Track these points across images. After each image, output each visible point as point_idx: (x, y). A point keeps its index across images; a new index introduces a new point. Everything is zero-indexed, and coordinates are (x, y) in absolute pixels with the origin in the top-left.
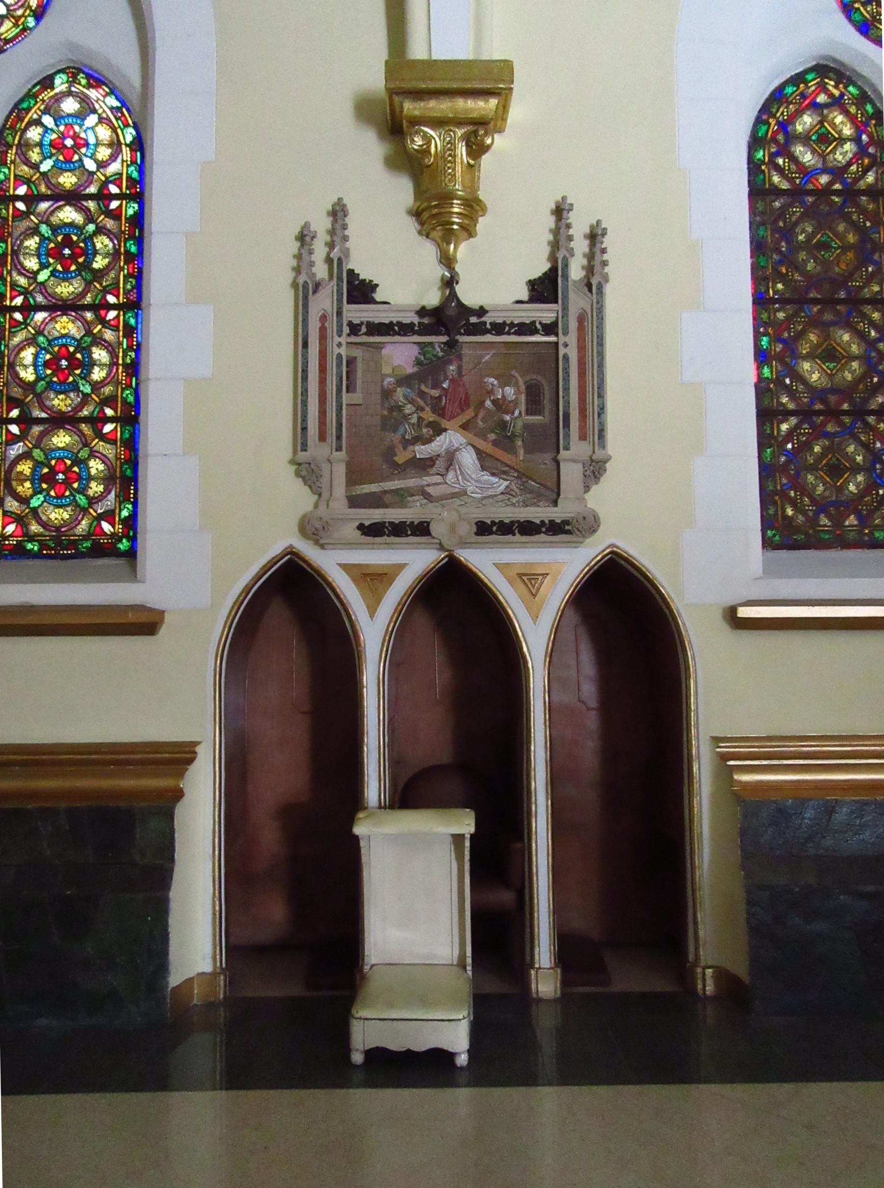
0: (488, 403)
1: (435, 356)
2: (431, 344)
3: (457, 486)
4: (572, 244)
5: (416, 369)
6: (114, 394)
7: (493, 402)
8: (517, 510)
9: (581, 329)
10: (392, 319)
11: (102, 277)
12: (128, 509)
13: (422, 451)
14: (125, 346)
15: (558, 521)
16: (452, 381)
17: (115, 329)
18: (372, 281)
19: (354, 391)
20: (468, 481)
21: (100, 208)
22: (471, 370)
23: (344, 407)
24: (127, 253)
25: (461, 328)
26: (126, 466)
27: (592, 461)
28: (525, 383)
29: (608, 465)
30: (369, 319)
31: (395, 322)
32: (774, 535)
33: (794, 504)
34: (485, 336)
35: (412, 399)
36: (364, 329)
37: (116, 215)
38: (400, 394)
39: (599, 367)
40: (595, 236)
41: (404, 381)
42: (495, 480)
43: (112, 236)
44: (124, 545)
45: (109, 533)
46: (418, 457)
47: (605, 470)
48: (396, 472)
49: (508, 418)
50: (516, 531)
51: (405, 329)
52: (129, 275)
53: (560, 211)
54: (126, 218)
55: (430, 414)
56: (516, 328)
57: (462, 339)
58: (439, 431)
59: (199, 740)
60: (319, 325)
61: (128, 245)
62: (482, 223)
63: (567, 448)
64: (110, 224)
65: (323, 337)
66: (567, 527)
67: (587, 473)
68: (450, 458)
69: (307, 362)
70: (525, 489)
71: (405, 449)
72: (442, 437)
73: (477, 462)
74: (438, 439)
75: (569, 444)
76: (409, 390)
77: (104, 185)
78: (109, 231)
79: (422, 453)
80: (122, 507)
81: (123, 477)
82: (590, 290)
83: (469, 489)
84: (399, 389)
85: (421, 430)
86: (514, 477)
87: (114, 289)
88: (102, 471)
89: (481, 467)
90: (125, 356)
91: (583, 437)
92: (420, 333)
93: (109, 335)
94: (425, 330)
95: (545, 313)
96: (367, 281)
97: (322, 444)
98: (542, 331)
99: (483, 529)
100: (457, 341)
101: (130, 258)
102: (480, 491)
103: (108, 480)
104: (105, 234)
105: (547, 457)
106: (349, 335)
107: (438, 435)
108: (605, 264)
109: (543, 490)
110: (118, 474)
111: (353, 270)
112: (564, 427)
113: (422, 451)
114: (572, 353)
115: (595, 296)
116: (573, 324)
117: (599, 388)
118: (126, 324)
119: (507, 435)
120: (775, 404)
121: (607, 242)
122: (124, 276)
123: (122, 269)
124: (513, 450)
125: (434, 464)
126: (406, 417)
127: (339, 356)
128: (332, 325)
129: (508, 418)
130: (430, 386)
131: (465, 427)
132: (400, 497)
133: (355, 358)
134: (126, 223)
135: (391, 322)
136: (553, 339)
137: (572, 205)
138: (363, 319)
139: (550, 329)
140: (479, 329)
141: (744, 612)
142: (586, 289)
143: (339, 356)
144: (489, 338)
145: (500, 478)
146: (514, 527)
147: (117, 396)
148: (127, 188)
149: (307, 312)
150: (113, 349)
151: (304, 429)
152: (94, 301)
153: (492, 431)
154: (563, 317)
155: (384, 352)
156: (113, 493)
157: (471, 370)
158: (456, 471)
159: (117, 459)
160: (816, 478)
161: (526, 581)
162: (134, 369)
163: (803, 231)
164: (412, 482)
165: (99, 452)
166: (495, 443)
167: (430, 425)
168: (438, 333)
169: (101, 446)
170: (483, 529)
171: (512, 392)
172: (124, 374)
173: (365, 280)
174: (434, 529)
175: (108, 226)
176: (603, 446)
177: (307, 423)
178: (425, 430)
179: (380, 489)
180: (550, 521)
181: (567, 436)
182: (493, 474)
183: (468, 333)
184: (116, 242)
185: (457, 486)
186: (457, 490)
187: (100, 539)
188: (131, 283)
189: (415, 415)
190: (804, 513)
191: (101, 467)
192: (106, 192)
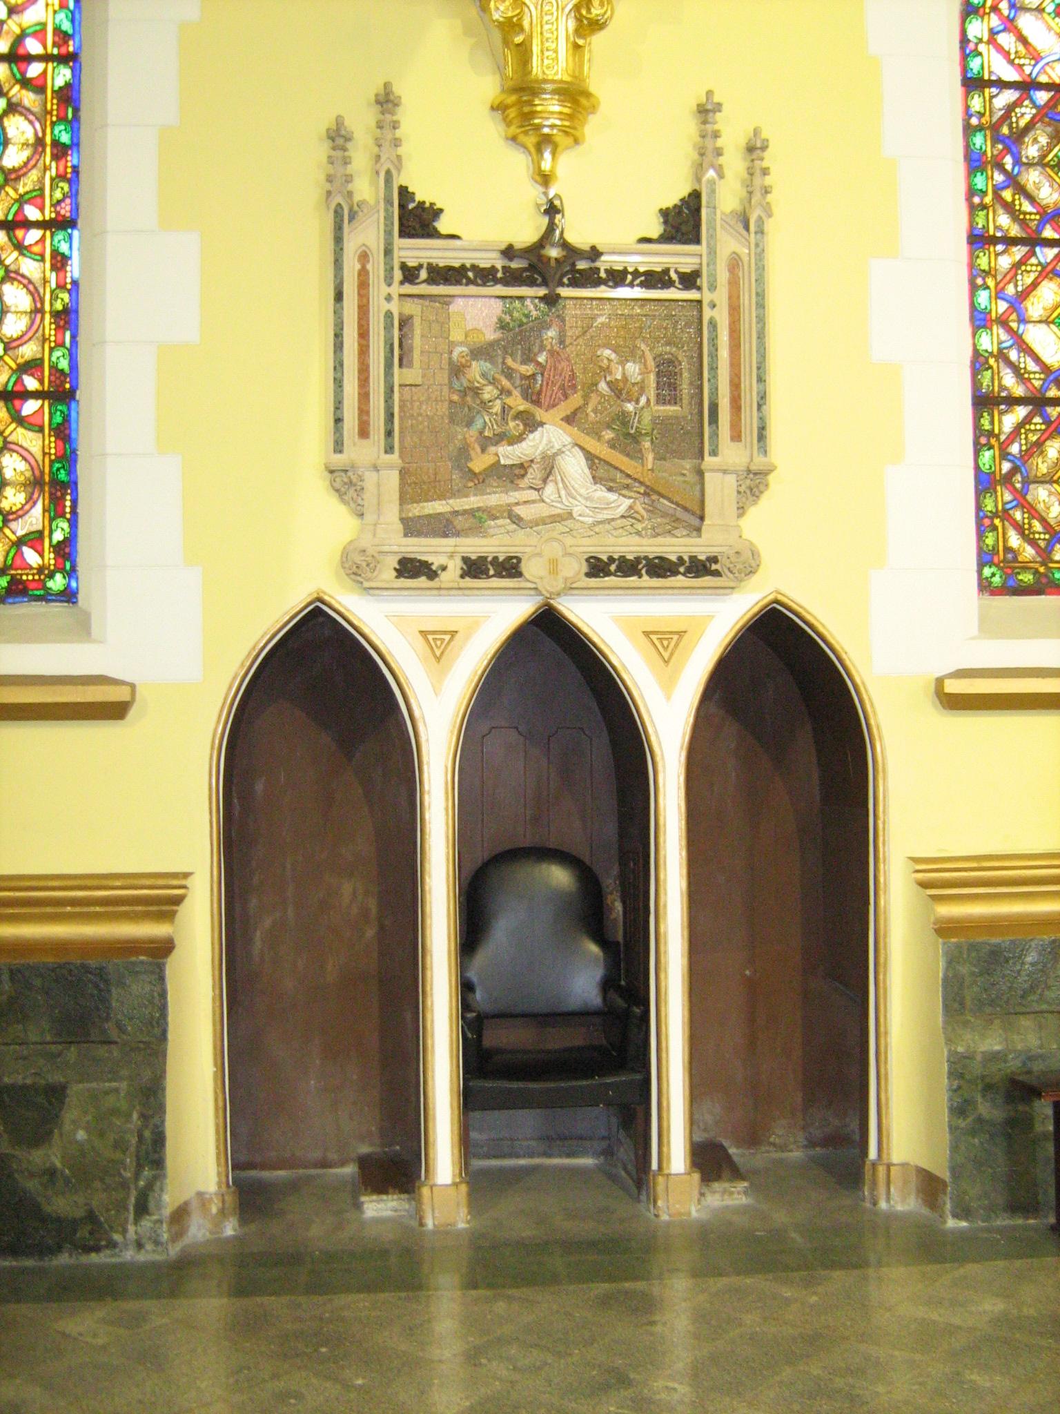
0: (603, 386)
1: (527, 316)
2: (521, 298)
3: (559, 505)
4: (721, 160)
5: (498, 335)
6: (39, 356)
7: (608, 384)
8: (645, 541)
9: (734, 283)
10: (465, 261)
11: (18, 178)
12: (63, 529)
13: (508, 454)
14: (54, 285)
15: (702, 557)
16: (552, 353)
17: (38, 258)
18: (434, 204)
19: (410, 365)
20: (574, 498)
21: (14, 75)
22: (578, 337)
23: (396, 389)
24: (56, 143)
25: (563, 276)
26: (57, 465)
27: (749, 471)
28: (654, 359)
29: (771, 478)
30: (431, 261)
31: (468, 266)
32: (993, 575)
33: (1019, 528)
34: (598, 289)
35: (494, 379)
36: (423, 274)
37: (38, 86)
38: (476, 370)
39: (758, 338)
40: (755, 149)
41: (481, 352)
42: (612, 496)
43: (31, 117)
44: (57, 583)
45: (35, 565)
46: (502, 462)
47: (767, 485)
48: (471, 484)
49: (630, 407)
50: (643, 572)
51: (485, 276)
52: (61, 177)
53: (706, 111)
54: (53, 91)
55: (520, 400)
56: (643, 278)
57: (564, 292)
58: (531, 424)
59: (190, 871)
60: (358, 267)
61: (56, 132)
62: (592, 128)
63: (714, 453)
64: (29, 98)
65: (363, 285)
66: (714, 567)
67: (742, 489)
68: (549, 466)
69: (342, 323)
70: (653, 510)
71: (483, 450)
72: (537, 434)
73: (587, 471)
74: (531, 436)
75: (717, 446)
76: (488, 365)
77: (19, 40)
78: (28, 110)
79: (508, 457)
80: (54, 527)
81: (55, 482)
82: (747, 228)
83: (575, 509)
84: (474, 363)
85: (507, 424)
86: (639, 493)
87: (36, 198)
88: (22, 473)
89: (594, 477)
90: (54, 297)
91: (736, 436)
92: (506, 282)
93: (30, 267)
94: (513, 278)
95: (679, 258)
96: (427, 205)
97: (365, 442)
98: (680, 283)
99: (597, 568)
100: (558, 296)
101: (60, 151)
102: (591, 513)
103: (35, 483)
104: (21, 114)
105: (687, 464)
106: (402, 283)
107: (531, 432)
108: (766, 191)
109: (680, 513)
110: (47, 478)
111: (407, 188)
112: (710, 423)
113: (508, 454)
114: (721, 316)
115: (752, 235)
116: (723, 276)
117: (759, 368)
118: (56, 253)
119: (629, 434)
120: (996, 389)
121: (770, 159)
122: (52, 180)
123: (46, 169)
124: (637, 455)
125: (526, 473)
126: (485, 405)
127: (389, 315)
128: (377, 268)
129: (630, 407)
130: (519, 358)
131: (569, 420)
132: (478, 520)
133: (411, 317)
134: (53, 98)
135: (463, 267)
136: (692, 295)
137: (719, 105)
138: (422, 261)
139: (690, 280)
140: (590, 279)
141: (952, 687)
142: (740, 227)
143: (389, 315)
144: (603, 292)
145: (620, 494)
146: (640, 566)
147: (42, 359)
148: (55, 44)
149: (342, 249)
150: (36, 288)
151: (338, 421)
152: (7, 215)
153: (609, 427)
154: (708, 265)
155: (452, 308)
156: (39, 505)
157: (578, 337)
158: (556, 483)
159: (44, 454)
160: (1050, 494)
161: (657, 642)
162: (67, 318)
163: (1035, 141)
164: (494, 499)
165: (17, 444)
166: (612, 445)
167: (519, 415)
168: (532, 283)
169: (22, 436)
170: (597, 568)
171: (637, 370)
172: (53, 326)
173: (424, 203)
174: (528, 568)
175: (26, 103)
176: (764, 450)
177: (342, 413)
178: (512, 424)
179: (448, 509)
180: (691, 557)
181: (715, 435)
182: (610, 489)
183: (574, 283)
184: (38, 126)
185: (559, 505)
186: (559, 511)
187: (21, 575)
188: (62, 189)
189: (498, 402)
190: (1033, 543)
191: (22, 466)
192: (21, 51)
